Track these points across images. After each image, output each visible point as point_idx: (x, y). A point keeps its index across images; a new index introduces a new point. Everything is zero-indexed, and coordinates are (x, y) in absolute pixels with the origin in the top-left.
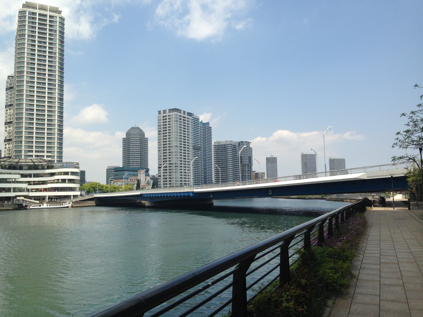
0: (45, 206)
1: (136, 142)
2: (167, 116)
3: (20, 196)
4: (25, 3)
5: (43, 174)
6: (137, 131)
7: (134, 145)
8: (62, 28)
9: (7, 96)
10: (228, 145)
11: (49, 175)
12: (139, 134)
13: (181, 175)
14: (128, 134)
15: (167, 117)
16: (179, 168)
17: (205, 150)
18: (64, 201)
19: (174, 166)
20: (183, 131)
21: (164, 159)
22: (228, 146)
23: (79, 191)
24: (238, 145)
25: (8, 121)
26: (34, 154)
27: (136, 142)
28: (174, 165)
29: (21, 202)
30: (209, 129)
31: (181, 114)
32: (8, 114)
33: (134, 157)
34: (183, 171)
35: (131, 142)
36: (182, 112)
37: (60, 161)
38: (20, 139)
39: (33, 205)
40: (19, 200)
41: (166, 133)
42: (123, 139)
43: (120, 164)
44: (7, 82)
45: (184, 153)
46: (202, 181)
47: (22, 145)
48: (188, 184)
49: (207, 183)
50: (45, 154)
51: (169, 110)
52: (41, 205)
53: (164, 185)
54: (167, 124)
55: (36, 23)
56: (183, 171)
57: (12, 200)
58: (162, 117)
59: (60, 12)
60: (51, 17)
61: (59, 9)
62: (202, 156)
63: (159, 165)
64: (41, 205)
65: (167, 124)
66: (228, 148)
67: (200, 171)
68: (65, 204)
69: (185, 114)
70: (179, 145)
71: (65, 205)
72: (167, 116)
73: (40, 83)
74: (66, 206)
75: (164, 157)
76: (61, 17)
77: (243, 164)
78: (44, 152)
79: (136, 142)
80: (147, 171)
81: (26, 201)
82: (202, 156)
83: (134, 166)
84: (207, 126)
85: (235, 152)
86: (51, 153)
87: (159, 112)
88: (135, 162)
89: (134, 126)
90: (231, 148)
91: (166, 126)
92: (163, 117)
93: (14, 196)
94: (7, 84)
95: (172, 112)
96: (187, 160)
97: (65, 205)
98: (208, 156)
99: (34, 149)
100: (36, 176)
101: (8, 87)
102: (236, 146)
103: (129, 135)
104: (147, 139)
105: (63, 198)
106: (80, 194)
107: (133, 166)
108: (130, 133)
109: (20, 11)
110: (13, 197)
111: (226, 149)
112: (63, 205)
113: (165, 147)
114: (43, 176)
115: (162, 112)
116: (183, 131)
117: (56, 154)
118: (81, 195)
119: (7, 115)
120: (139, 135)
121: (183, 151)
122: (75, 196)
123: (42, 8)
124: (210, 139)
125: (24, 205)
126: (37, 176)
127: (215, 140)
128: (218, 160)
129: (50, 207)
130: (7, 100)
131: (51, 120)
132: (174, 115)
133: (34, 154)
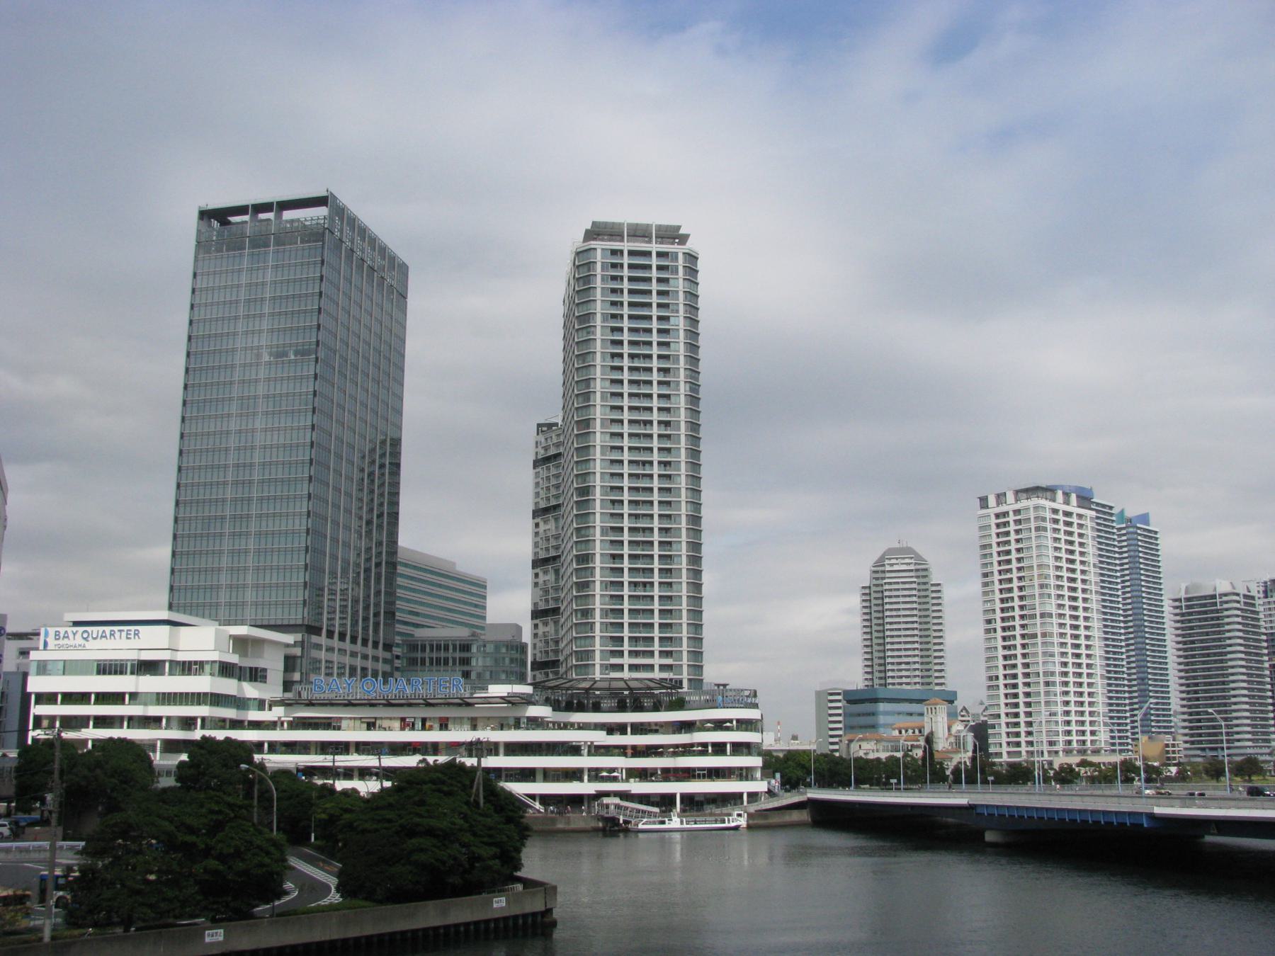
0: (675, 822)
3: (607, 794)
4: (589, 227)
5: (656, 724)
6: (907, 561)
8: (692, 281)
10: (1226, 595)
12: (911, 571)
14: (879, 570)
15: (1011, 518)
16: (1059, 689)
17: (1139, 626)
18: (725, 810)
20: (1068, 569)
21: (1005, 657)
22: (1225, 599)
23: (762, 780)
24: (1262, 595)
26: (626, 660)
28: (1042, 679)
29: (612, 812)
30: (1151, 538)
31: (1055, 505)
34: (1072, 698)
37: (697, 683)
39: (645, 820)
40: (607, 806)
43: (854, 676)
44: (537, 443)
46: (1123, 576)
47: (594, 637)
48: (1092, 741)
50: (657, 661)
51: (1017, 492)
52: (666, 819)
55: (622, 278)
56: (1072, 698)
57: (586, 804)
58: (993, 517)
59: (683, 239)
61: (681, 232)
62: (1134, 686)
64: (666, 819)
66: (1225, 606)
67: (1125, 669)
68: (731, 818)
69: (1068, 504)
70: (1054, 611)
71: (729, 820)
72: (1011, 513)
74: (733, 824)
75: (1004, 596)
76: (687, 251)
78: (651, 654)
80: (950, 699)
81: (626, 808)
82: (1134, 686)
85: (1253, 619)
86: (672, 656)
87: (984, 502)
90: (1238, 605)
92: (997, 516)
93: (594, 793)
94: (537, 447)
95: (1027, 499)
97: (729, 820)
98: (1154, 657)
99: (626, 647)
100: (639, 729)
101: (540, 457)
102: (1253, 598)
106: (766, 790)
109: (579, 250)
111: (1217, 611)
112: (723, 822)
114: (656, 731)
116: (1068, 569)
117: (685, 661)
118: (770, 793)
122: (753, 796)
123: (639, 232)
124: (1161, 640)
125: (621, 822)
126: (642, 730)
127: (1173, 587)
129: (688, 826)
130: (537, 494)
131: (670, 556)
133: (626, 660)
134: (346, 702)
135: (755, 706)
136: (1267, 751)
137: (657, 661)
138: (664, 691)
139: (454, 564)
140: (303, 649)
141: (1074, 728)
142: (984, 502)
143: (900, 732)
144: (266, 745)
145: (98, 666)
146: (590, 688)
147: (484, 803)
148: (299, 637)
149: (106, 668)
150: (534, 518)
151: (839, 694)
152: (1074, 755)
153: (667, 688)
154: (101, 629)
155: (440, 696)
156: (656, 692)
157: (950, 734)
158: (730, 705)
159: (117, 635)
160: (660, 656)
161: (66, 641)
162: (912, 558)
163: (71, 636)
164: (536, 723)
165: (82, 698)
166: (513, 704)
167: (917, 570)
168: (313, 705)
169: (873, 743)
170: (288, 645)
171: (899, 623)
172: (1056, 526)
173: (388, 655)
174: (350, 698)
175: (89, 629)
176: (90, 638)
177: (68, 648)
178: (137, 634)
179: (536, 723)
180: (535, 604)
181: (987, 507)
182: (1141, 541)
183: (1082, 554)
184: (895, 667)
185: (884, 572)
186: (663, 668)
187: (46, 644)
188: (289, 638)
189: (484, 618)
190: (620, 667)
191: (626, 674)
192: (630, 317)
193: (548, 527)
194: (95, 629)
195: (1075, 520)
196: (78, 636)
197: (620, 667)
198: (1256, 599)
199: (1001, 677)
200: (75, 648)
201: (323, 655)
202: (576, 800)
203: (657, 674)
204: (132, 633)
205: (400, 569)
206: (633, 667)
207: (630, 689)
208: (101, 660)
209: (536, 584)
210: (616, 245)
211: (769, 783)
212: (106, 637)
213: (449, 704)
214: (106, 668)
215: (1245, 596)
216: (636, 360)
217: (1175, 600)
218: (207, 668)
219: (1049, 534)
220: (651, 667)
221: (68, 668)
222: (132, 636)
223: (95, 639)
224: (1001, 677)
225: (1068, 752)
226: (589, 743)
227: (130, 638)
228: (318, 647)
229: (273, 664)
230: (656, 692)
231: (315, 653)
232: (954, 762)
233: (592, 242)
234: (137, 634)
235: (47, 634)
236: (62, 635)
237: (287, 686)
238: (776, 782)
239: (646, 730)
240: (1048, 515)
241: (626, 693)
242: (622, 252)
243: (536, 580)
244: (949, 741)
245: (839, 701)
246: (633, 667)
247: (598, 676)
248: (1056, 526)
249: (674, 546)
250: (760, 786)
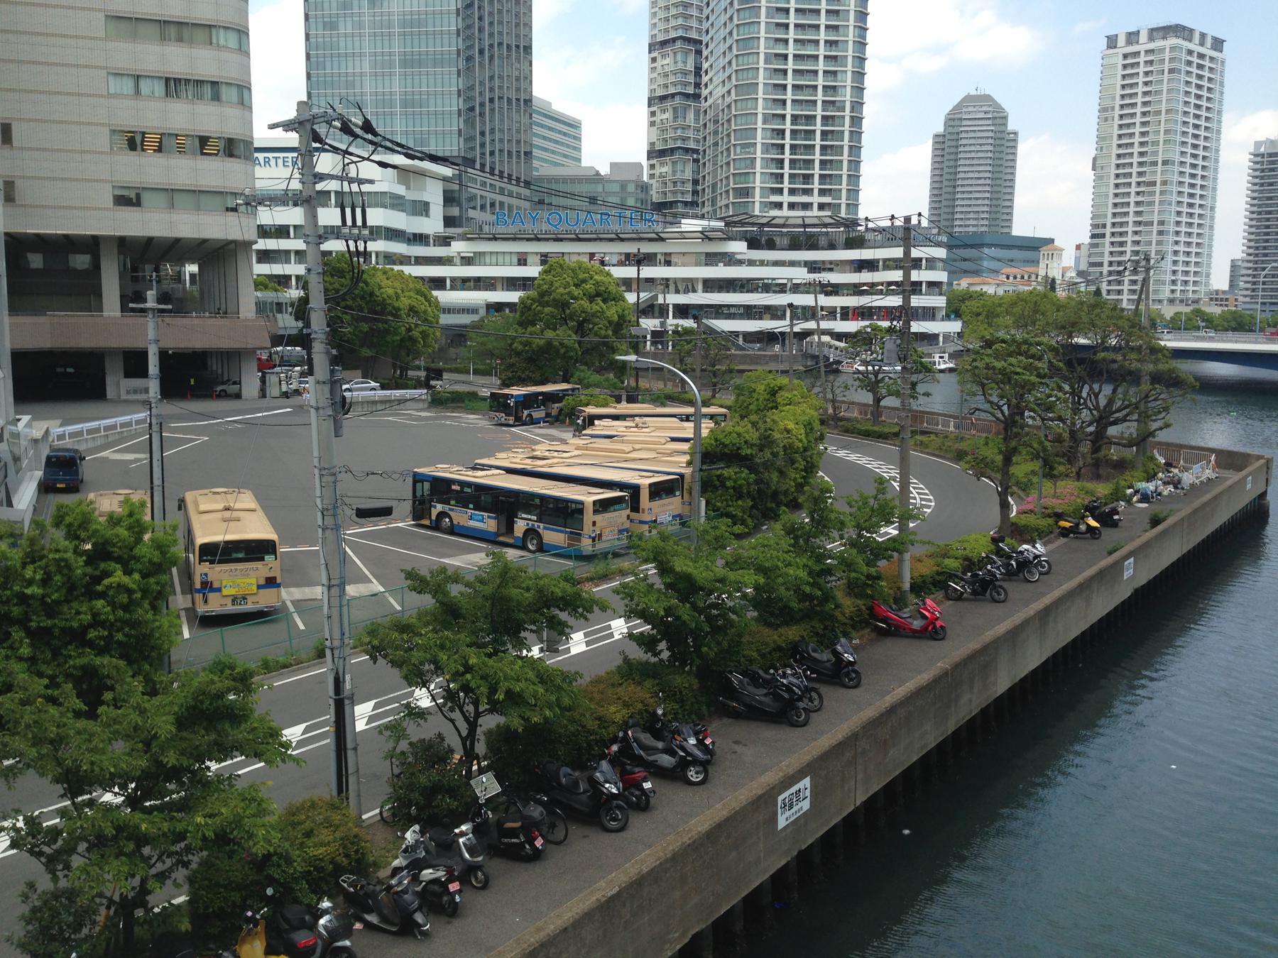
1: (981, 145)
2: (1142, 53)
5: (831, 262)
7: (973, 158)
9: (654, 14)
11: (848, 268)
12: (989, 118)
19: (1155, 233)
26: (786, 198)
27: (978, 148)
31: (1191, 46)
32: (659, 70)
33: (970, 199)
35: (964, 146)
36: (1197, 38)
38: (749, 153)
41: (1133, 115)
42: (936, 136)
50: (816, 199)
51: (1152, 30)
58: (1121, 57)
63: (1095, 226)
72: (1142, 53)
79: (978, 148)
83: (969, 226)
87: (1112, 42)
88: (972, 216)
89: (973, 93)
92: (1125, 56)
99: (786, 185)
103: (957, 123)
104: (1015, 133)
107: (966, 226)
108: (959, 116)
114: (831, 270)
115: (1121, 41)
119: (655, 75)
120: (989, 122)
128: (1267, 205)
132: (1168, 50)
133: (786, 198)
137: (816, 199)
139: (550, 104)
143: (1008, 278)
144: (448, 282)
147: (1086, 337)
150: (650, 52)
159: (273, 162)
160: (820, 195)
164: (730, 260)
167: (995, 118)
168: (496, 239)
180: (652, 144)
181: (1115, 47)
185: (961, 119)
188: (447, 171)
189: (579, 160)
190: (779, 205)
191: (785, 212)
193: (665, 62)
197: (779, 205)
199: (1109, 225)
202: (770, 338)
204: (290, 160)
206: (792, 206)
209: (652, 124)
213: (601, 239)
224: (1109, 225)
229: (433, 194)
237: (449, 221)
239: (820, 268)
240: (1185, 57)
246: (792, 206)
247: (757, 212)
248: (1188, 69)
249: (839, 76)
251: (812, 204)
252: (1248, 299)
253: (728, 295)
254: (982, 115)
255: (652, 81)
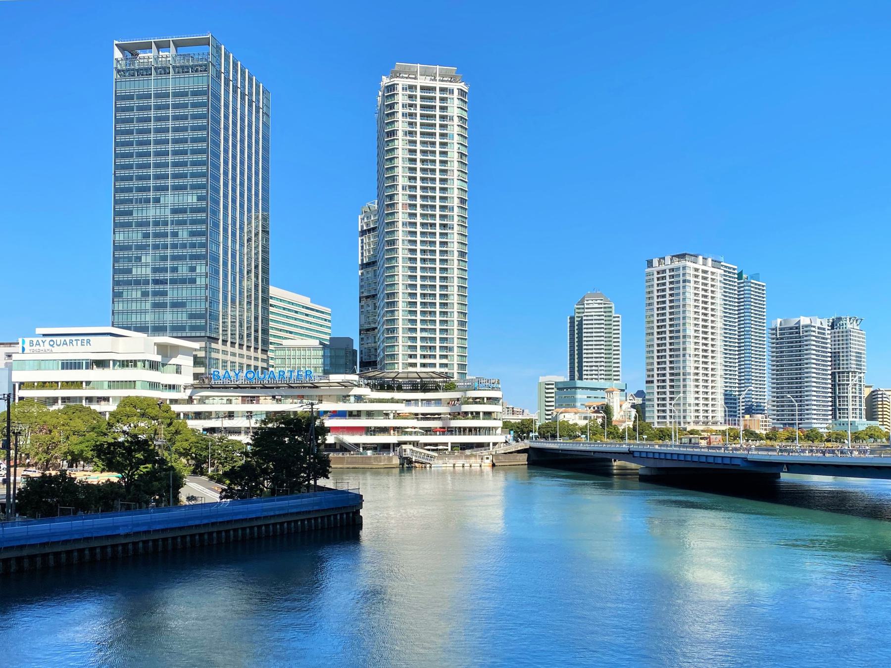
3: (405, 443)
6: (598, 301)
12: (601, 308)
13: (697, 386)
15: (668, 274)
25: (366, 326)
26: (419, 361)
40: (405, 450)
45: (703, 326)
49: (753, 411)
53: (658, 377)
54: (666, 283)
58: (655, 273)
60: (443, 90)
65: (666, 283)
73: (426, 224)
75: (660, 324)
77: (841, 370)
78: (434, 357)
84: (753, 283)
91: (664, 281)
96: (710, 366)
102: (824, 329)
105: (476, 447)
110: (394, 444)
113: (662, 351)
116: (703, 320)
121: (701, 335)
133: (419, 361)
134: (236, 386)
135: (498, 389)
136: (825, 426)
138: (442, 380)
140: (206, 352)
141: (701, 408)
142: (650, 264)
145: (63, 364)
146: (395, 377)
148: (203, 344)
149: (68, 365)
151: (553, 384)
152: (700, 425)
153: (444, 378)
154: (63, 338)
155: (298, 382)
156: (437, 380)
157: (621, 410)
158: (483, 388)
159: (75, 343)
160: (440, 358)
161: (38, 347)
162: (602, 300)
163: (41, 343)
165: (53, 385)
166: (345, 386)
169: (572, 414)
170: (196, 350)
171: (592, 341)
172: (696, 280)
173: (265, 357)
174: (238, 383)
175: (54, 339)
176: (55, 345)
177: (39, 352)
178: (89, 342)
179: (359, 399)
182: (753, 291)
183: (713, 298)
184: (589, 368)
186: (442, 365)
187: (23, 349)
188: (196, 345)
190: (414, 365)
191: (418, 369)
192: (422, 133)
194: (58, 339)
195: (709, 276)
196: (47, 343)
197: (414, 365)
198: (826, 330)
200: (45, 352)
201: (220, 356)
202: (386, 447)
203: (438, 369)
204: (85, 341)
205: (271, 302)
206: (424, 365)
207: (420, 378)
208: (64, 360)
210: (412, 82)
211: (506, 437)
212: (66, 344)
214: (68, 365)
215: (819, 328)
216: (425, 163)
217: (773, 329)
218: (139, 364)
219: (692, 284)
220: (434, 365)
221: (40, 365)
222: (85, 344)
223: (59, 345)
225: (697, 423)
226: (394, 412)
227: (84, 345)
228: (217, 351)
230: (437, 380)
231: (214, 355)
232: (623, 428)
233: (395, 79)
234: (89, 342)
235: (24, 342)
236: (35, 343)
238: (510, 437)
241: (419, 380)
242: (416, 87)
243: (362, 310)
244: (621, 414)
245: (553, 389)
246: (424, 365)
247: (400, 370)
248: (696, 280)
250: (501, 439)
251: (416, 364)
252: (775, 421)
253: (478, 437)
254: (597, 306)
255: (361, 287)
